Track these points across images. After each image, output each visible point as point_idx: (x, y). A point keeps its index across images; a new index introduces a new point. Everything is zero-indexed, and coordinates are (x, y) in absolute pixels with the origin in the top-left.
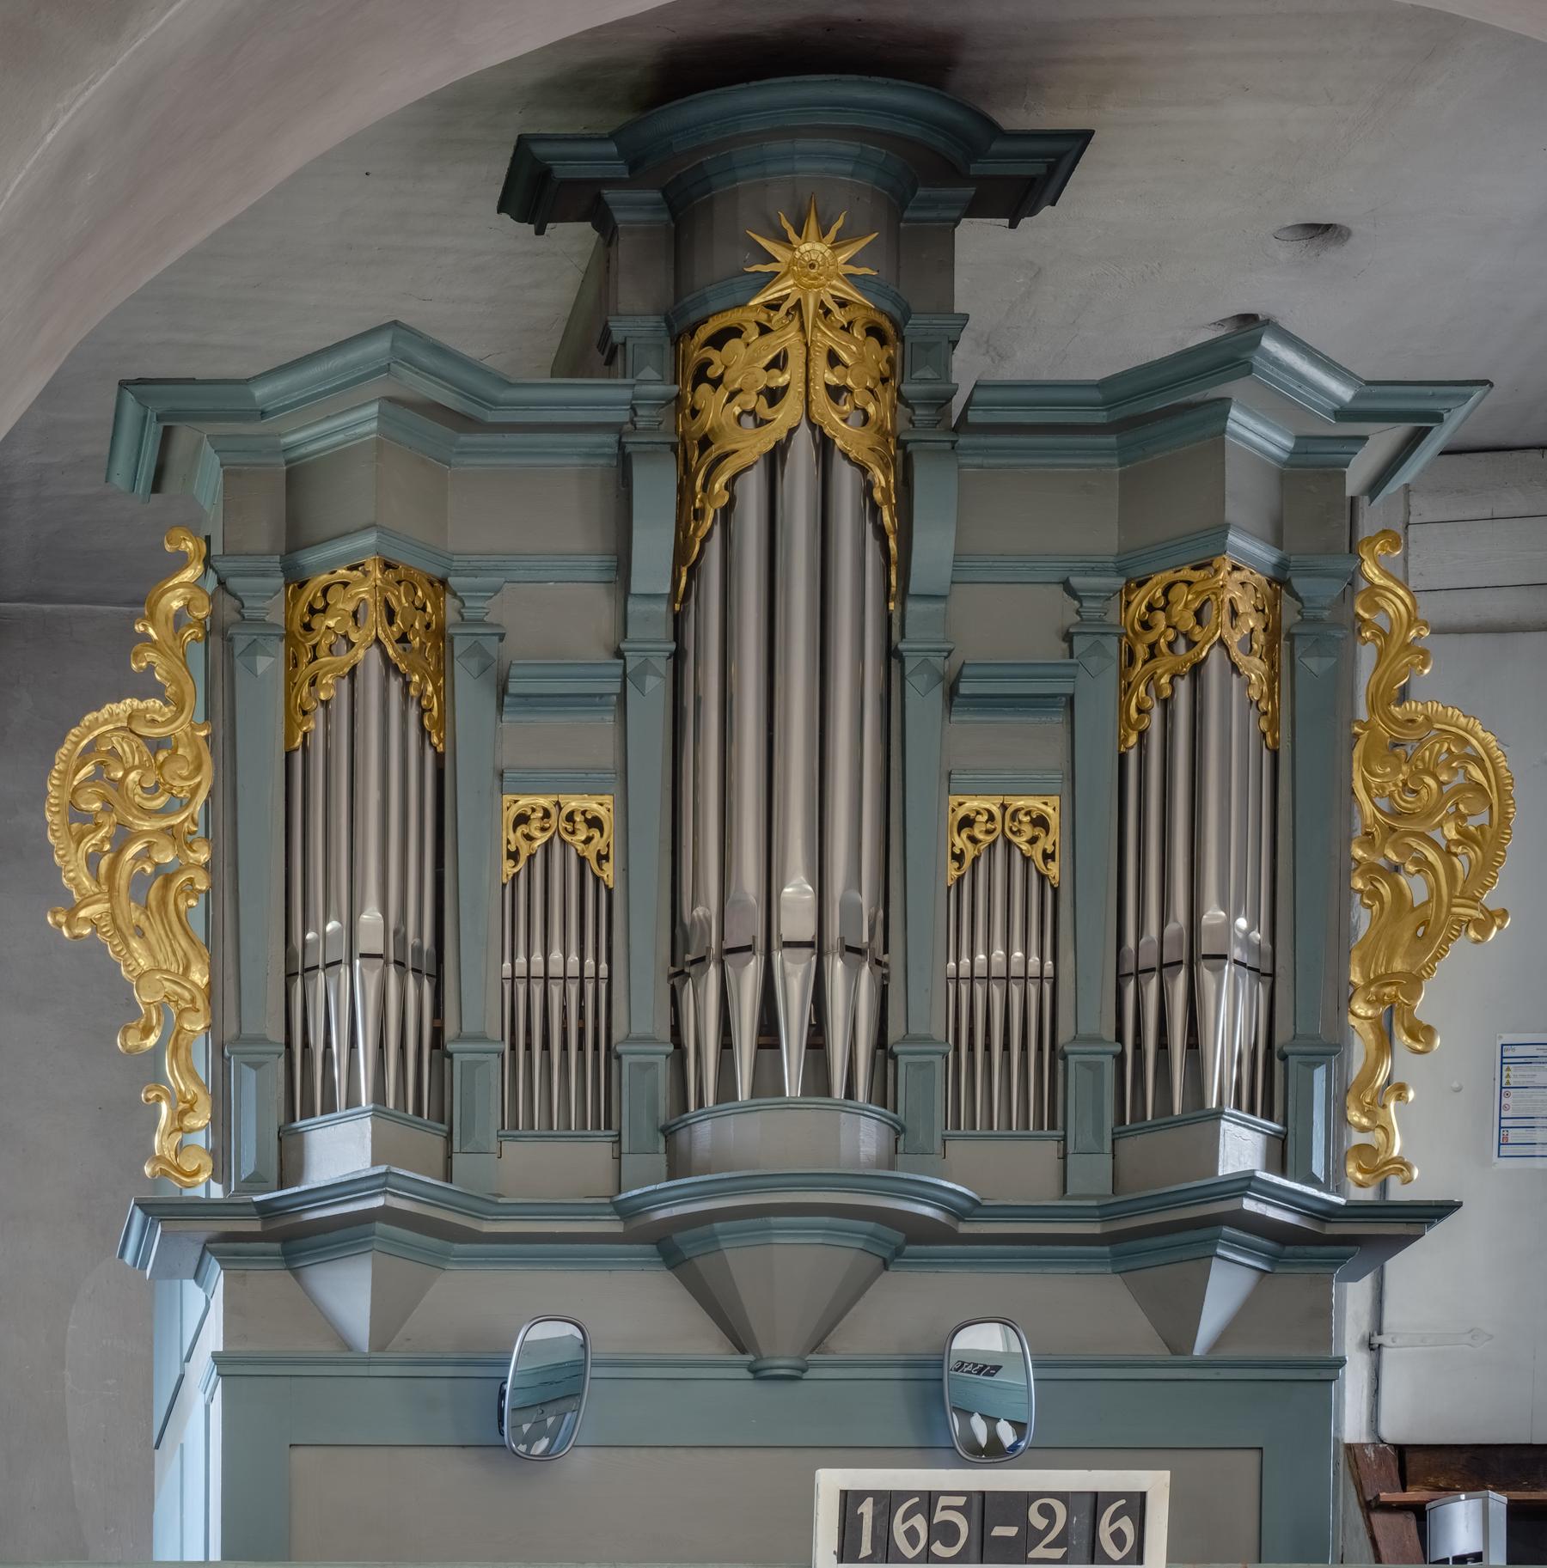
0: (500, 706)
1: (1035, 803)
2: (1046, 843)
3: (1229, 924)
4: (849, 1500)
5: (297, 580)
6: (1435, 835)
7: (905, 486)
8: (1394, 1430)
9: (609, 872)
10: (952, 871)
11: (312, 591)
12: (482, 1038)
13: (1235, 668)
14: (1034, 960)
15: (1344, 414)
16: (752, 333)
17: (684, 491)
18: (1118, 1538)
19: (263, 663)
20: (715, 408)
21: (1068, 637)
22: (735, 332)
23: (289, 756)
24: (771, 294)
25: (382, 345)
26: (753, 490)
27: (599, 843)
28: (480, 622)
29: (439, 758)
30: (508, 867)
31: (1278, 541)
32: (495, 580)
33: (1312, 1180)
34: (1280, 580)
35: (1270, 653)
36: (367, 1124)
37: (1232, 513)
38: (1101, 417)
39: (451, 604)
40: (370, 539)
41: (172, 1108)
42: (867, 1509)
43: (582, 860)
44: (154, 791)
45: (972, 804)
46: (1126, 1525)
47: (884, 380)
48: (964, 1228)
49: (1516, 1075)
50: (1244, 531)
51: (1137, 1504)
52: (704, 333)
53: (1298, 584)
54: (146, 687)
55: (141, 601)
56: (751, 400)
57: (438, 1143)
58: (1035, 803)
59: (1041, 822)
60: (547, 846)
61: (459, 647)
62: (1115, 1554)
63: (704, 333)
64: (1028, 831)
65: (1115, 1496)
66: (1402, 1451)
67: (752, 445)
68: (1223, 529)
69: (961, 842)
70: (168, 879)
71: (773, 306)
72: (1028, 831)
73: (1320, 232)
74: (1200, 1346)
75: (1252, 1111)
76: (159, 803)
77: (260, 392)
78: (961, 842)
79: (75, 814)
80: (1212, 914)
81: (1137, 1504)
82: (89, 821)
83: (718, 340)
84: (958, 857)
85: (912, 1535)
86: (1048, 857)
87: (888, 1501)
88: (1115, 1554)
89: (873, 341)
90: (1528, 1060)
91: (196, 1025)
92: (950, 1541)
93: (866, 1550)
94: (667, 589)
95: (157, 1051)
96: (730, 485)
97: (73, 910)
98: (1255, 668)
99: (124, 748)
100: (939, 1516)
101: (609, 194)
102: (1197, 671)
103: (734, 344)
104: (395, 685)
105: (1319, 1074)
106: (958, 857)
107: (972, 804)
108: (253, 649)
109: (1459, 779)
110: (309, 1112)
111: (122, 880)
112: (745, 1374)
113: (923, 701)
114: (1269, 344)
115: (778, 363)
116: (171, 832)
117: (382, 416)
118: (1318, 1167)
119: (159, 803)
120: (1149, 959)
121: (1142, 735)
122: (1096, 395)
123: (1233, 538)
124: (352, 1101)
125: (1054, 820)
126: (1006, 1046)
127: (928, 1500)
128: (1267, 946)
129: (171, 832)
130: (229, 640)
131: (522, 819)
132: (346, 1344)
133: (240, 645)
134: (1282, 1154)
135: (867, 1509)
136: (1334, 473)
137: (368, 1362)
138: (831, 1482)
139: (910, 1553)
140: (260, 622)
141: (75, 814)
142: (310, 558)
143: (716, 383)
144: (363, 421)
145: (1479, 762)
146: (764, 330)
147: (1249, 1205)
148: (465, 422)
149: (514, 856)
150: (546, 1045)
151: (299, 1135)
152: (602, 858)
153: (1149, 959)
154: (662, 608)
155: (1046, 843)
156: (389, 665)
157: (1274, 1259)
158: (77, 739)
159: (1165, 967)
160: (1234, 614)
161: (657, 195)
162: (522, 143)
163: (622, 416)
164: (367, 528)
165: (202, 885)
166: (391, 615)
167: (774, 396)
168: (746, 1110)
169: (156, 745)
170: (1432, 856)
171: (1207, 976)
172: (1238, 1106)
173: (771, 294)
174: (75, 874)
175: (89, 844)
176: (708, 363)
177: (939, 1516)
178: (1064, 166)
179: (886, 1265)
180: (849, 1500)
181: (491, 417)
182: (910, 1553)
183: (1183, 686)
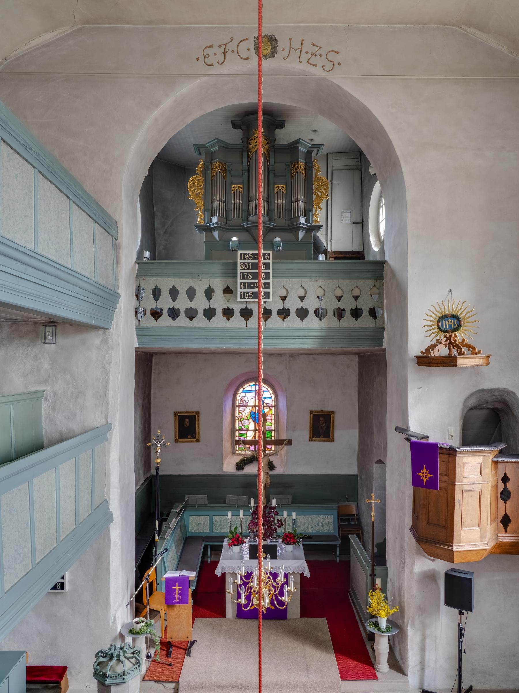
0: (231, 176)
1: (283, 186)
2: (284, 190)
3: (301, 197)
4: (241, 254)
5: (212, 163)
6: (322, 189)
7: (269, 155)
8: (333, 250)
9: (242, 193)
10: (275, 192)
11: (213, 165)
12: (230, 209)
13: (301, 172)
14: (282, 201)
15: (310, 148)
16: (254, 140)
17: (248, 155)
18: (267, 257)
19: (208, 172)
20: (251, 147)
21: (286, 169)
22: (252, 139)
23: (211, 181)
24: (255, 135)
25: (216, 140)
26: (254, 154)
27: (241, 189)
28: (229, 168)
29: (226, 181)
30: (232, 192)
31: (306, 160)
32: (231, 164)
33: (310, 223)
34: (306, 164)
35: (305, 171)
36: (217, 218)
37: (300, 157)
38: (287, 148)
39: (227, 166)
40: (217, 160)
41: (200, 216)
42: (242, 255)
43: (240, 191)
44: (198, 185)
45: (277, 186)
46: (268, 256)
47: (267, 144)
48: (275, 228)
49: (344, 214)
50: (301, 159)
51: (269, 254)
52: (250, 139)
53: (307, 164)
54: (197, 174)
55: (197, 167)
56: (254, 146)
57: (225, 219)
58: (283, 186)
59: (283, 187)
60: (236, 190)
61: (227, 170)
62: (267, 259)
63: (250, 139)
64: (282, 188)
65: (267, 253)
66: (334, 252)
67: (254, 150)
68: (299, 159)
69: (276, 189)
70: (200, 193)
71: (255, 137)
72: (282, 188)
73: (315, 131)
74: (299, 240)
75: (304, 216)
76: (199, 186)
77: (207, 145)
78: (276, 189)
79: (190, 187)
80: (299, 197)
81: (269, 254)
82: (192, 188)
83: (251, 140)
84: (276, 191)
85: (247, 257)
86: (284, 191)
87: (244, 254)
88: (267, 259)
89: (265, 140)
90: (345, 212)
91: (202, 208)
92: (251, 258)
93: (243, 259)
94: (247, 164)
95: (198, 210)
96: (252, 154)
97: (190, 196)
98: (303, 172)
99: (195, 180)
100: (250, 255)
101: (241, 126)
102: (297, 172)
103: (252, 140)
104: (221, 174)
105: (310, 213)
106: (276, 191)
107: (277, 186)
108: (207, 170)
109: (324, 183)
110: (213, 216)
111: (195, 193)
112: (255, 243)
113: (272, 176)
114: (300, 140)
115: (256, 142)
116: (200, 189)
117: (218, 148)
118: (310, 222)
119: (199, 186)
120: (294, 201)
121: (293, 179)
122: (286, 146)
123: (300, 159)
124: (217, 215)
125: (285, 187)
126: (281, 210)
127: (248, 254)
128: (305, 200)
129: (200, 189)
130: (205, 170)
131: (234, 187)
132: (216, 240)
133: (206, 170)
134: (307, 221)
135: (242, 255)
136: (311, 154)
137: (219, 242)
138: (239, 252)
139: (247, 259)
140: (208, 168)
141: (190, 187)
142: (213, 161)
143: (251, 144)
144: (217, 148)
145: (326, 182)
146: (255, 139)
147: (301, 225)
148: (227, 148)
149: (233, 191)
150: (236, 210)
151: (212, 219)
152: (241, 191)
153: (294, 201)
154: (247, 166)
155: (284, 190)
156: (220, 172)
157: (306, 231)
158: (190, 180)
159: (295, 202)
160: (301, 167)
161: (246, 126)
162: (232, 121)
163: (242, 147)
164: (217, 159)
165: (203, 194)
166: (220, 167)
167: (256, 145)
168: (254, 216)
169: (198, 180)
170: (321, 191)
171: (299, 203)
172: (303, 216)
173: (255, 135)
174: (190, 193)
175: (191, 190)
176: (250, 142)
177: (250, 255)
178: (284, 123)
179: (269, 232)
180: (241, 254)
181: (229, 148)
182: (247, 259)
183: (296, 174)
